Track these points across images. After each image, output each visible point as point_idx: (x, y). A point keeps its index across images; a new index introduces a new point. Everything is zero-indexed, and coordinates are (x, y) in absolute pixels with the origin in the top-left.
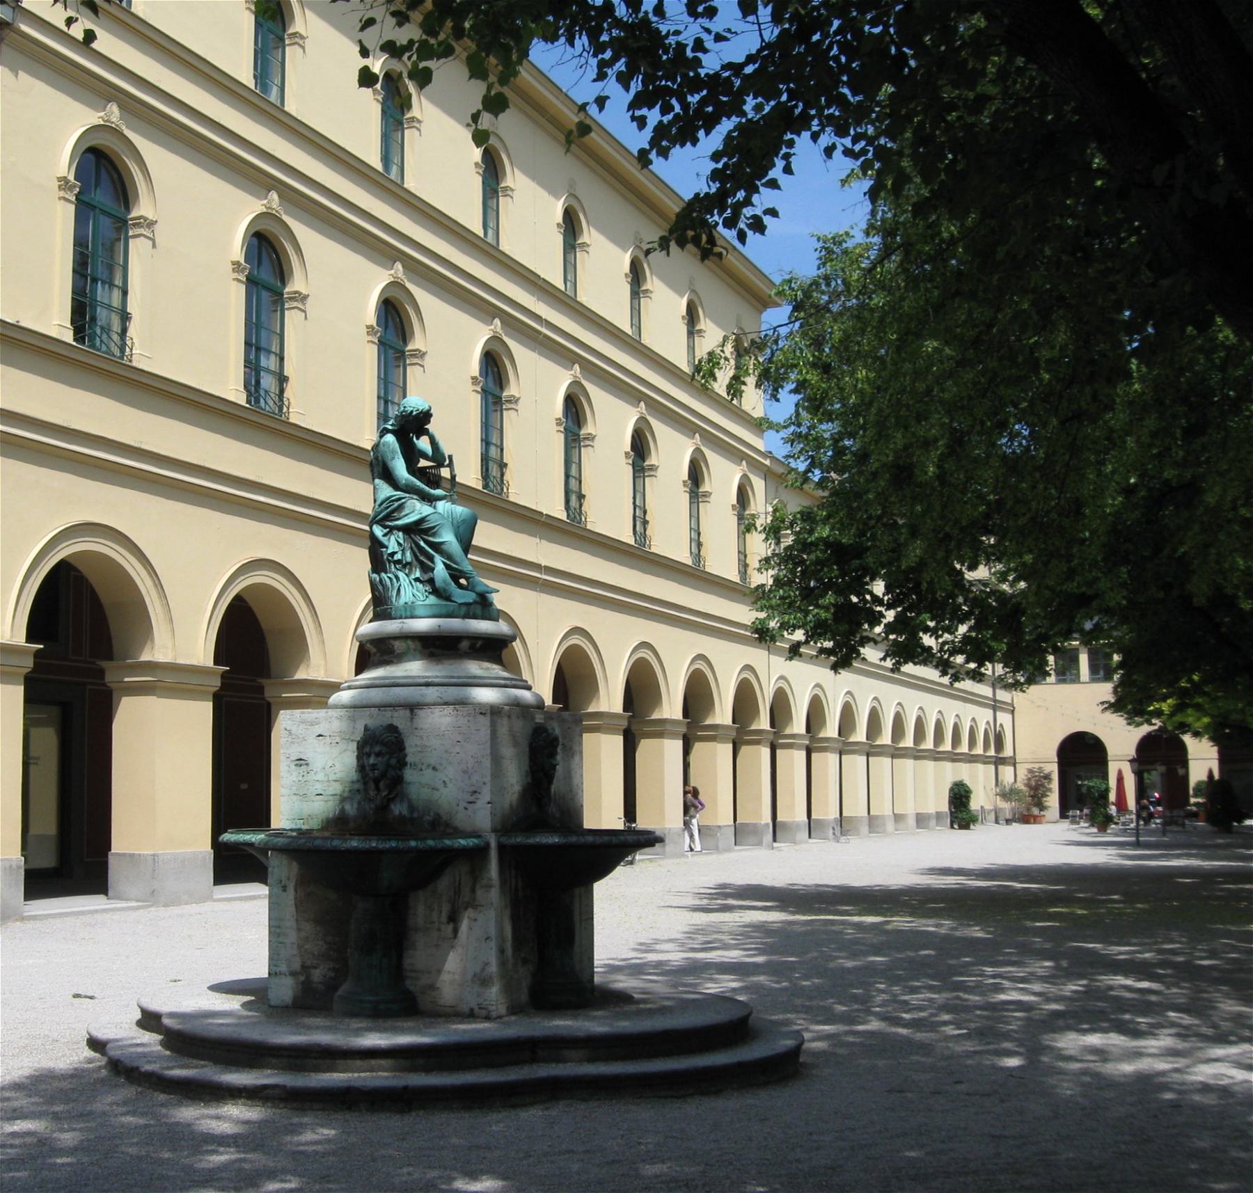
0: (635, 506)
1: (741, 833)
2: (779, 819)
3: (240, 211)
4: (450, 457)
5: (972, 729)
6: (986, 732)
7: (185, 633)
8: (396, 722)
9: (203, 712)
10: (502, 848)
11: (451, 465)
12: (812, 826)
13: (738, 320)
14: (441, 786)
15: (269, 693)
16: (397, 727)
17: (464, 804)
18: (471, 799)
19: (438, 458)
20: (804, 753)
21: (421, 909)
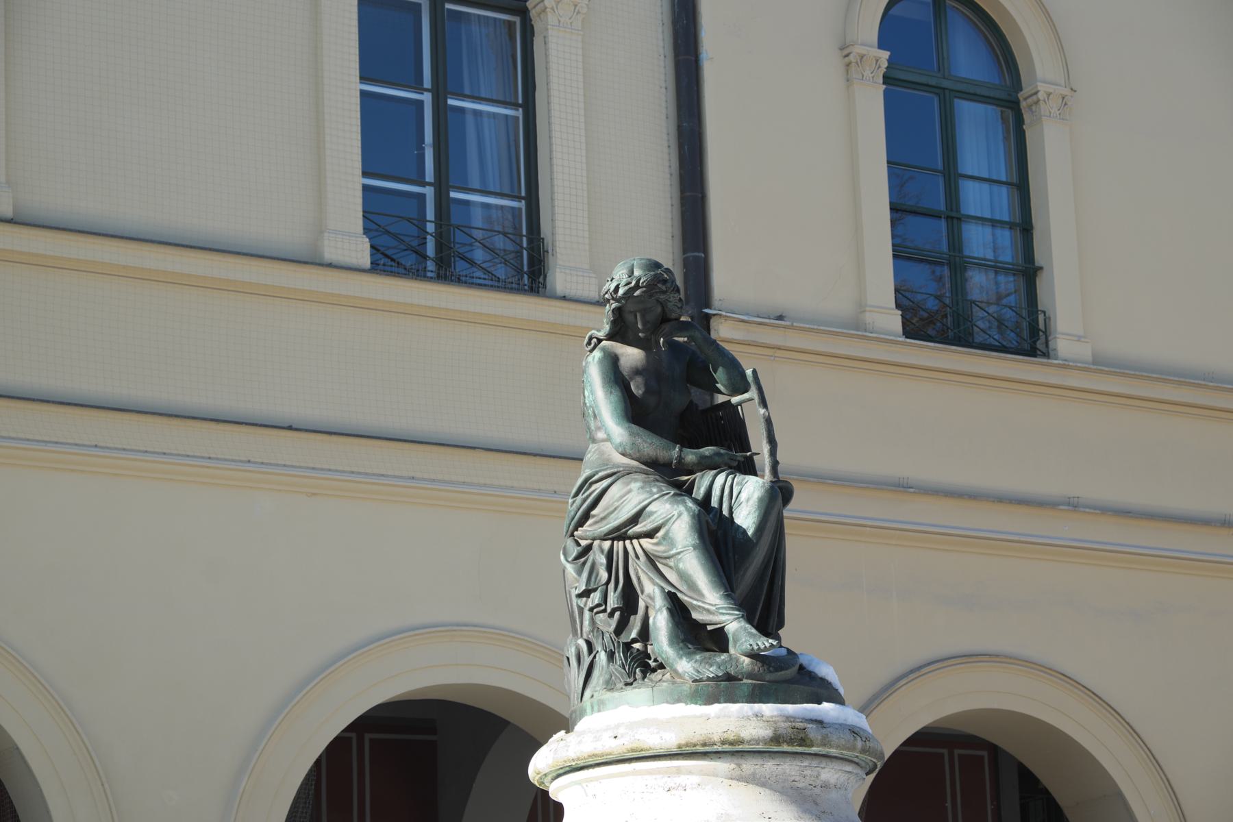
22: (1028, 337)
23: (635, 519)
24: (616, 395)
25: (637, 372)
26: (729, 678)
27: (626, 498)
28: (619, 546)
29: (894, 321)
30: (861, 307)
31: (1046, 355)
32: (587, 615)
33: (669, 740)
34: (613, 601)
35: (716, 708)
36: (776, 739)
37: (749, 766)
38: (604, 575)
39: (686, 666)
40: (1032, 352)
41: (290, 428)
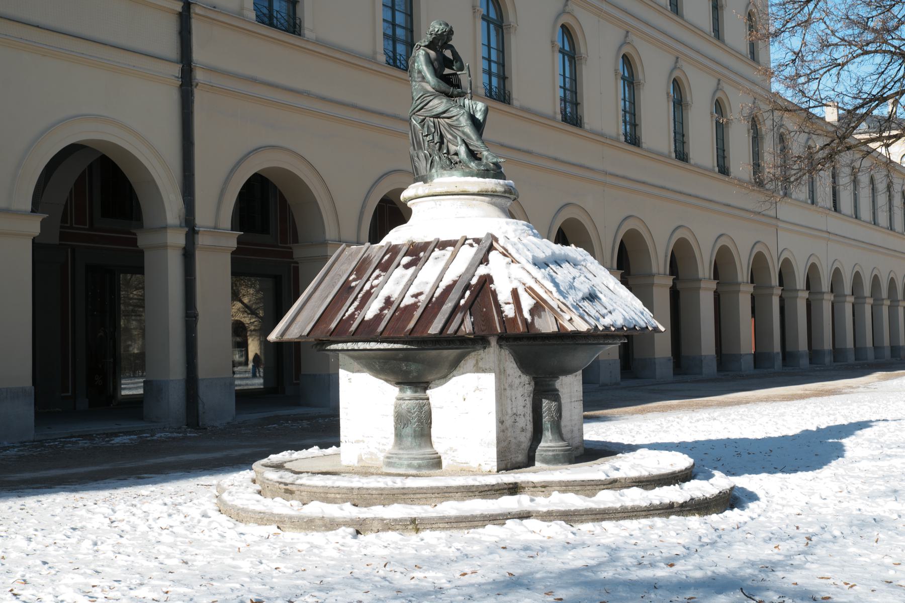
22: (294, 27)
23: (444, 112)
24: (431, 68)
25: (436, 60)
26: (487, 170)
27: (439, 104)
28: (436, 120)
29: (252, 15)
30: (242, 8)
31: (300, 35)
32: (426, 143)
33: (476, 189)
34: (437, 139)
35: (487, 180)
36: (505, 192)
37: (495, 200)
38: (433, 130)
39: (473, 165)
40: (294, 33)
41: (38, 27)
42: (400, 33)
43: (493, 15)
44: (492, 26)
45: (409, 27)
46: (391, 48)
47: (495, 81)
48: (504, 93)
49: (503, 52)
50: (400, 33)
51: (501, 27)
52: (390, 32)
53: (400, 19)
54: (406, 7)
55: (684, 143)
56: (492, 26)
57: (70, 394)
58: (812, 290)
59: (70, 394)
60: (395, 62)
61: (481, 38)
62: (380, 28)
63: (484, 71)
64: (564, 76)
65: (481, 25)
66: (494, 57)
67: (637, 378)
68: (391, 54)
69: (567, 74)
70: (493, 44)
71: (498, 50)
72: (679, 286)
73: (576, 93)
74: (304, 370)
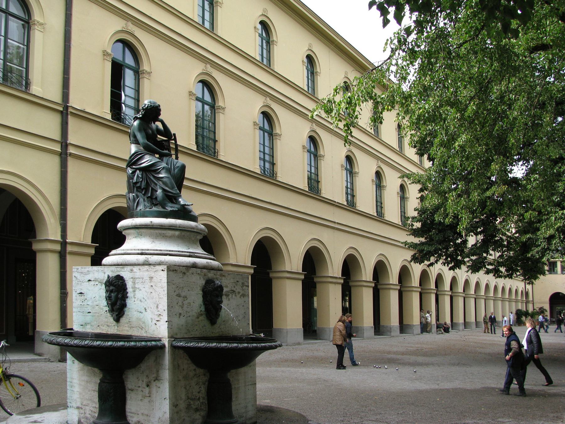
0: (377, 201)
1: (425, 327)
2: (454, 321)
3: (257, 104)
4: (174, 135)
5: (516, 290)
6: (522, 291)
7: (293, 261)
8: (123, 274)
9: (299, 285)
10: (174, 348)
11: (175, 139)
12: (466, 324)
13: (346, 73)
14: (144, 311)
15: (271, 275)
16: (122, 277)
17: (154, 322)
18: (158, 319)
19: (166, 132)
20: (474, 299)
21: (132, 380)
42: (267, 158)
43: (313, 149)
44: (312, 155)
45: (137, 98)
46: (262, 165)
47: (267, 165)
48: (273, 172)
49: (273, 149)
50: (267, 158)
51: (28, 23)
52: (262, 157)
53: (267, 150)
54: (270, 145)
55: (382, 207)
56: (312, 155)
57: (4, 333)
58: (454, 291)
59: (4, 333)
60: (264, 172)
61: (306, 161)
62: (258, 155)
63: (260, 159)
64: (264, 145)
65: (306, 155)
66: (313, 171)
67: (320, 339)
68: (263, 168)
69: (349, 181)
70: (313, 164)
71: (315, 167)
72: (379, 287)
73: (273, 157)
74: (381, 324)
